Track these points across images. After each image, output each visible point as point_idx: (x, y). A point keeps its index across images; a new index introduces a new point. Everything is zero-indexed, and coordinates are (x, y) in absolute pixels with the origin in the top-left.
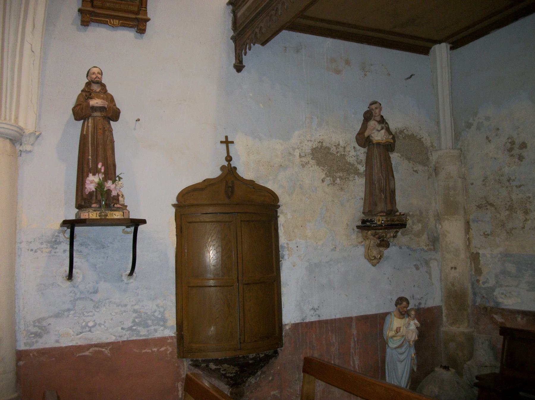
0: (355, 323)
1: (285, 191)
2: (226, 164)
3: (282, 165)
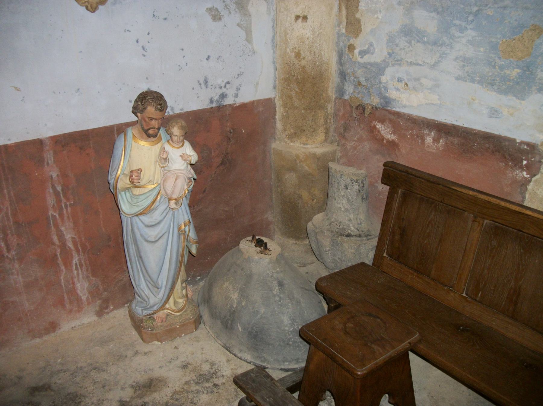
0: (51, 153)
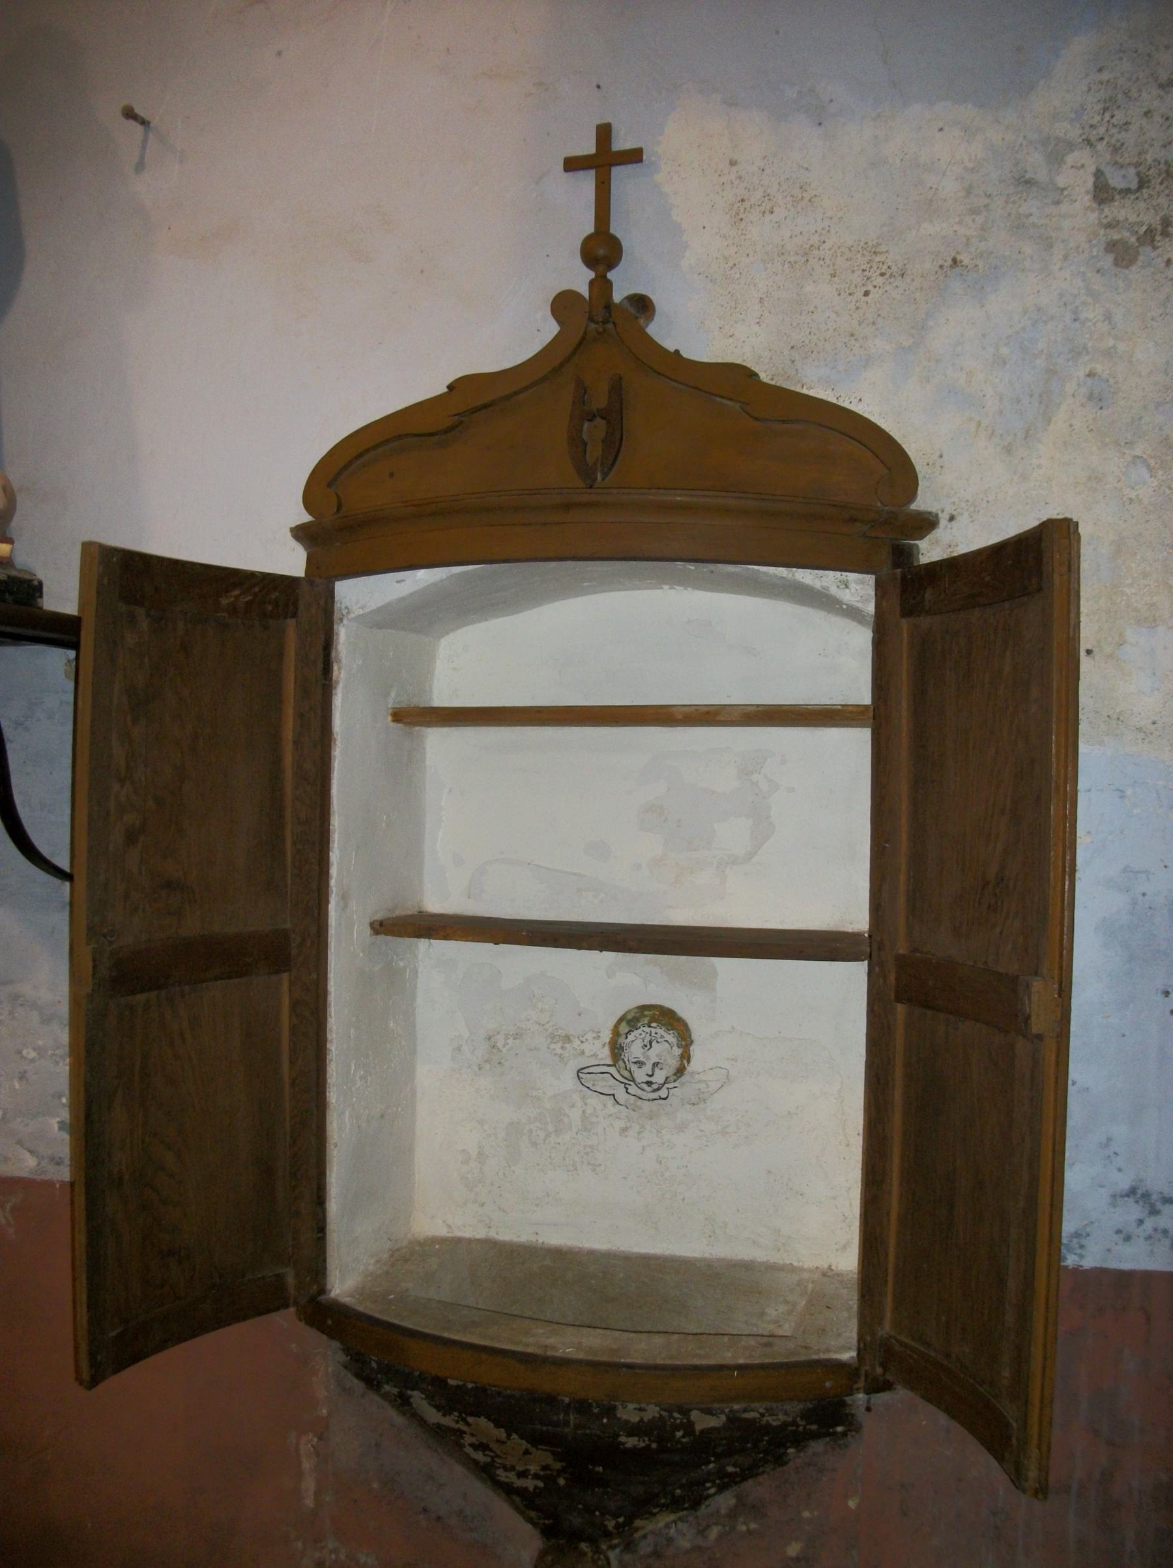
1: (979, 424)
2: (580, 279)
3: (965, 258)
